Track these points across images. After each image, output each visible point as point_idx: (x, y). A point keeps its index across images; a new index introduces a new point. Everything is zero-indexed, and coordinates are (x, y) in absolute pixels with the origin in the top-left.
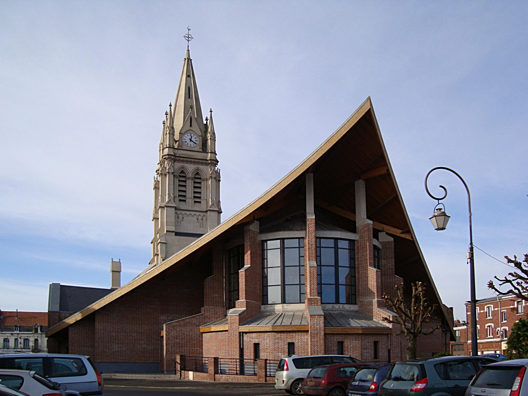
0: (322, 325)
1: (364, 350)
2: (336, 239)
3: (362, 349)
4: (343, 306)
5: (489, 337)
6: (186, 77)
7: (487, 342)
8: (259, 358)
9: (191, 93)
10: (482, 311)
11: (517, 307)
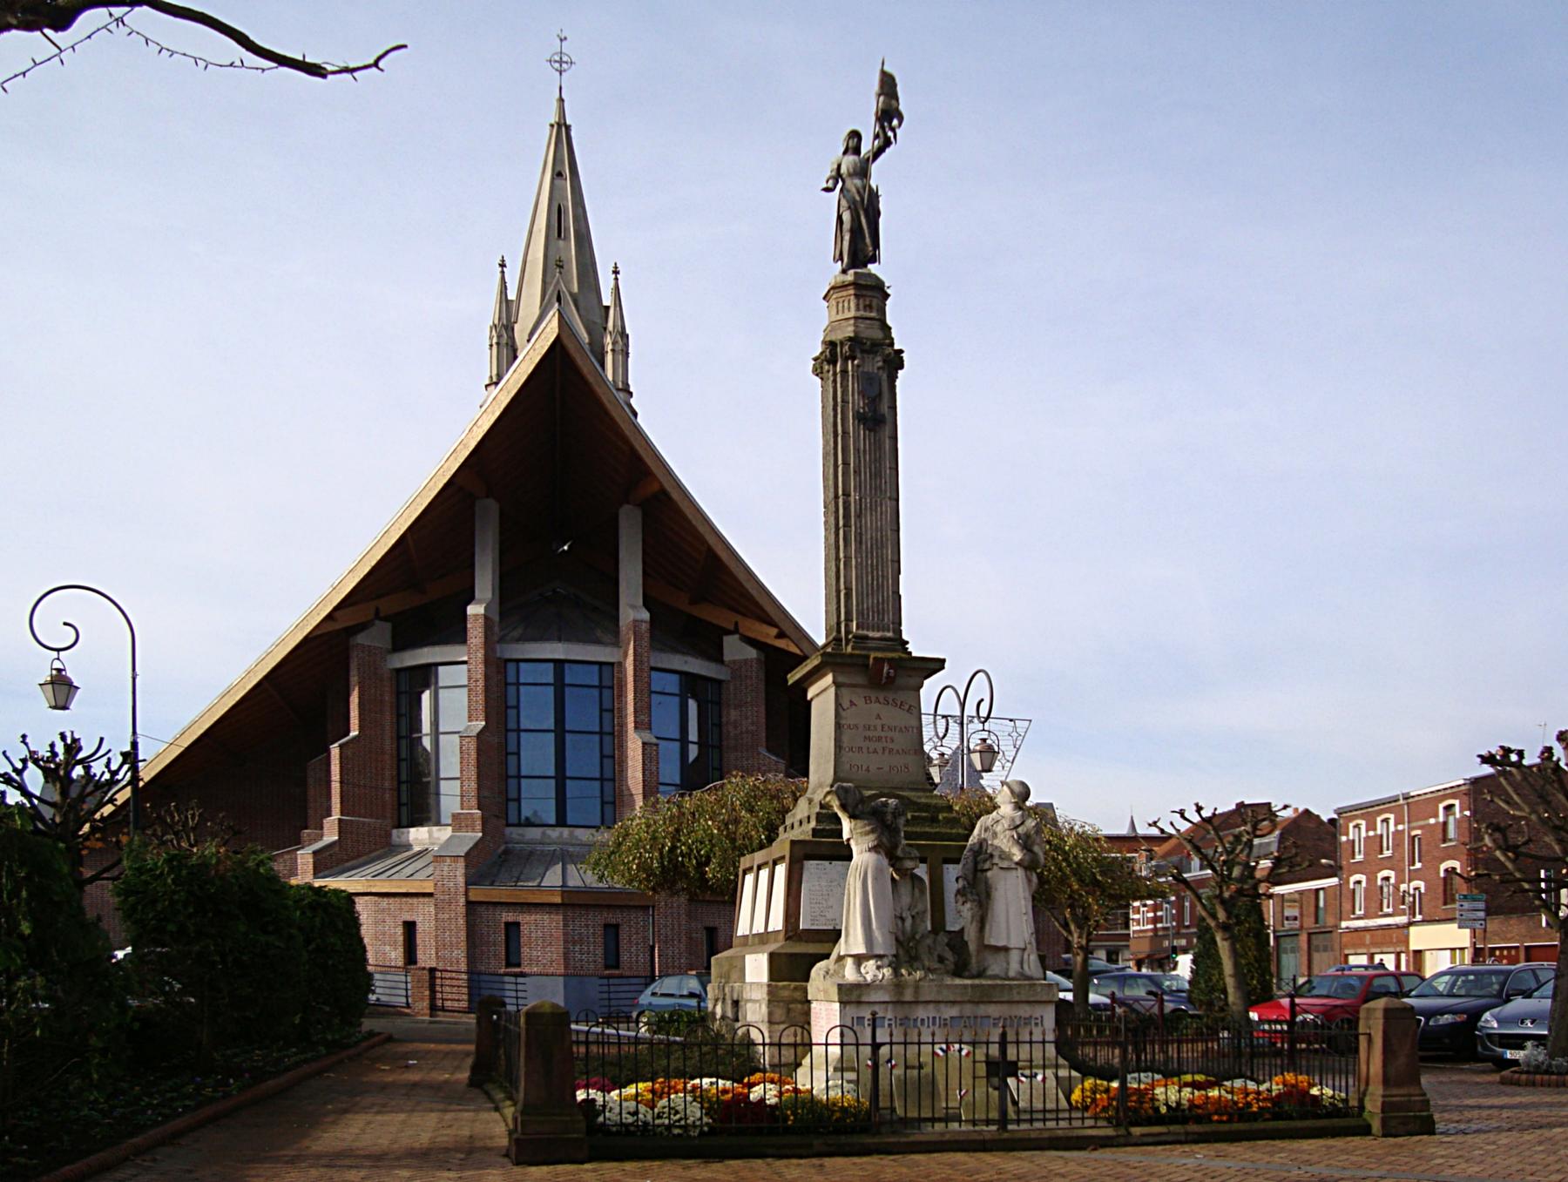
0: (461, 880)
1: (574, 943)
2: (560, 664)
3: (566, 942)
4: (571, 834)
5: (1386, 910)
6: (553, 179)
7: (1381, 928)
8: (415, 963)
9: (567, 223)
10: (1371, 833)
11: (1445, 824)
